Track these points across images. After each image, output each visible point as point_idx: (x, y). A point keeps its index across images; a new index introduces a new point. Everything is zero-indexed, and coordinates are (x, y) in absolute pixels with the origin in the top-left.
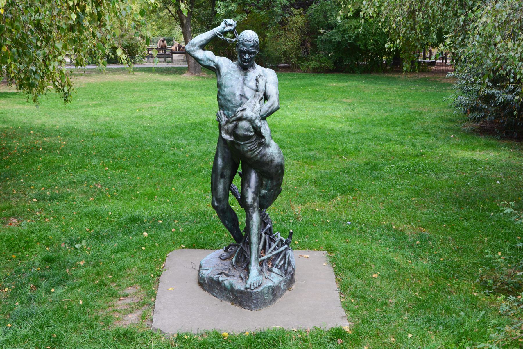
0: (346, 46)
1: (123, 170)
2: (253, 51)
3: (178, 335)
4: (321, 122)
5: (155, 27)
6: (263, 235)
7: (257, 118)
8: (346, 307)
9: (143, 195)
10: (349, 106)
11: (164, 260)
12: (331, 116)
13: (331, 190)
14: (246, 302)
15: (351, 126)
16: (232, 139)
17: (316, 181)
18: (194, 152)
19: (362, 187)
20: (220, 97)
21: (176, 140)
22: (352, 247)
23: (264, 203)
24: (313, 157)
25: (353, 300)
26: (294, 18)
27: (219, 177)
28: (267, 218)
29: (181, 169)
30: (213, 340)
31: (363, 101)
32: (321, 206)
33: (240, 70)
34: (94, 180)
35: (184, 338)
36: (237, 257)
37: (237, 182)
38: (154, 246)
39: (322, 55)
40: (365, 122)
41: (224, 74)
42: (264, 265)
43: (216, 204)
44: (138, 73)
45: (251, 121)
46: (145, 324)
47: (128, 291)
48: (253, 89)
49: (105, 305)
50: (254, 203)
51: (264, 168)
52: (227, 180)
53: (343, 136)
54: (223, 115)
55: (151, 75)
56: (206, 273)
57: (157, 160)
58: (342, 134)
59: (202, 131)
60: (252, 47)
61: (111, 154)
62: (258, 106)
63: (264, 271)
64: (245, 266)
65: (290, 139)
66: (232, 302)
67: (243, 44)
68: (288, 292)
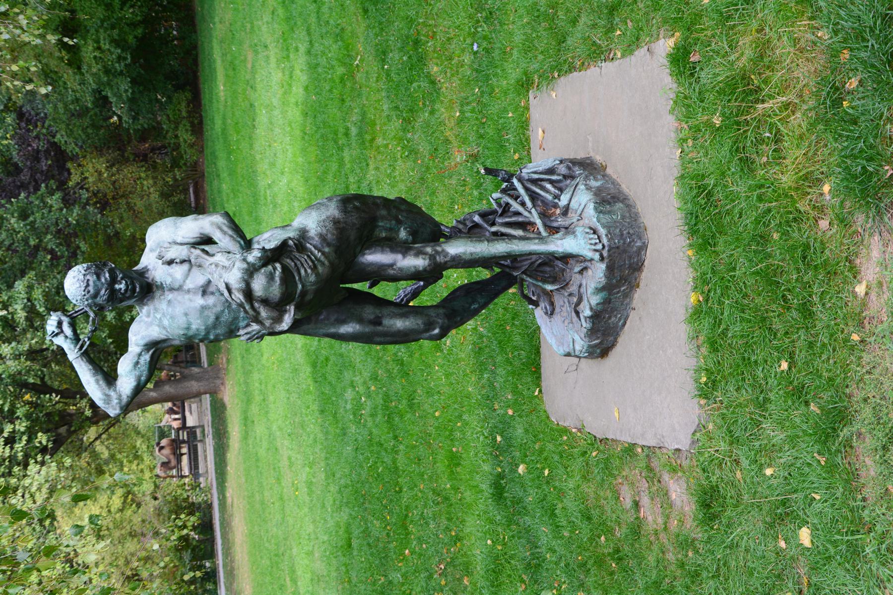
0: (141, 66)
1: (408, 520)
2: (107, 275)
3: (700, 396)
4: (295, 114)
5: (134, 467)
6: (494, 229)
7: (245, 260)
8: (633, 44)
9: (452, 476)
10: (260, 56)
11: (566, 431)
12: (281, 92)
13: (419, 87)
14: (630, 257)
15: (297, 49)
16: (292, 308)
17: (404, 119)
18: (366, 374)
19: (410, 21)
21: (346, 411)
22: (518, 38)
23: (428, 232)
24: (360, 128)
25: (619, 32)
26: (91, 180)
27: (380, 328)
28: (462, 222)
30: (707, 322)
31: (248, 26)
32: (450, 108)
33: (153, 298)
34: (430, 577)
35: (706, 384)
36: (545, 281)
37: (384, 290)
38: (541, 451)
39: (165, 117)
40: (288, 19)
41: (164, 332)
42: (555, 224)
43: (437, 331)
44: (228, 495)
45: (251, 271)
46: (686, 463)
47: (628, 503)
48: (190, 270)
49: (655, 548)
50: (425, 254)
51: (352, 238)
52: (386, 311)
53: (318, 65)
55: (231, 469)
56: (580, 344)
57: (386, 450)
58: (313, 67)
59: (327, 359)
60: (98, 278)
61: (381, 545)
62: (219, 258)
63: (567, 223)
64: (560, 264)
65: (330, 177)
66: (634, 286)
67: (96, 295)
68: (609, 171)
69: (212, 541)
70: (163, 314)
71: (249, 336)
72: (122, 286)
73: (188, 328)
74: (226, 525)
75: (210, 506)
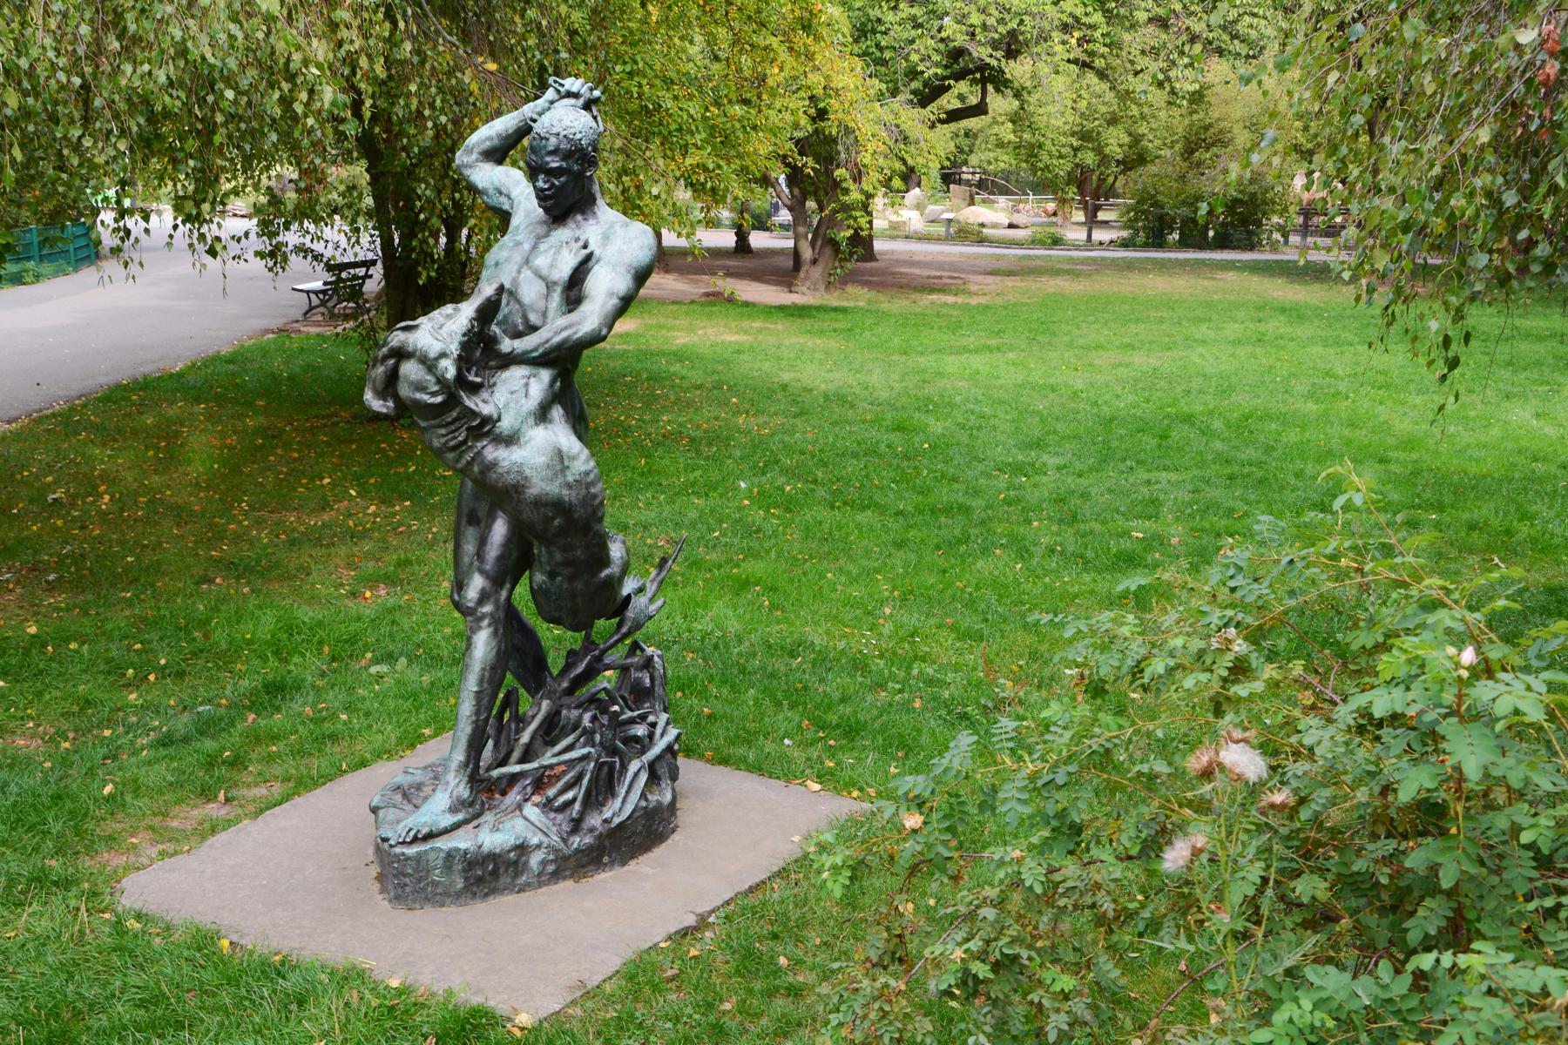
2: (555, 165)
27: (464, 522)
69: (1203, 245)
75: (1251, 247)
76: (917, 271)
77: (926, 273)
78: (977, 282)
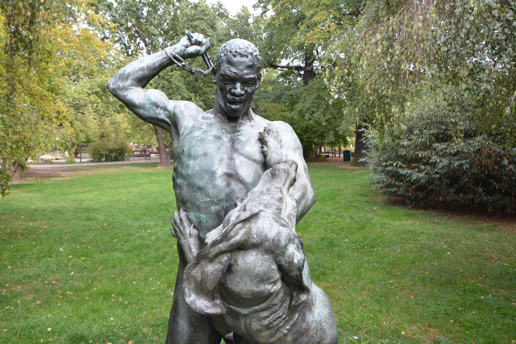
7: (290, 240)
18: (160, 235)
20: (179, 181)
21: (145, 221)
29: (145, 255)
33: (223, 122)
41: (186, 132)
45: (273, 250)
48: (254, 161)
54: (186, 224)
55: (133, 168)
59: (169, 212)
67: (230, 63)
69: (111, 161)
70: (206, 132)
71: (178, 221)
72: (238, 89)
73: (190, 156)
74: (116, 166)
76: (41, 172)
77: (46, 172)
78: (63, 174)
